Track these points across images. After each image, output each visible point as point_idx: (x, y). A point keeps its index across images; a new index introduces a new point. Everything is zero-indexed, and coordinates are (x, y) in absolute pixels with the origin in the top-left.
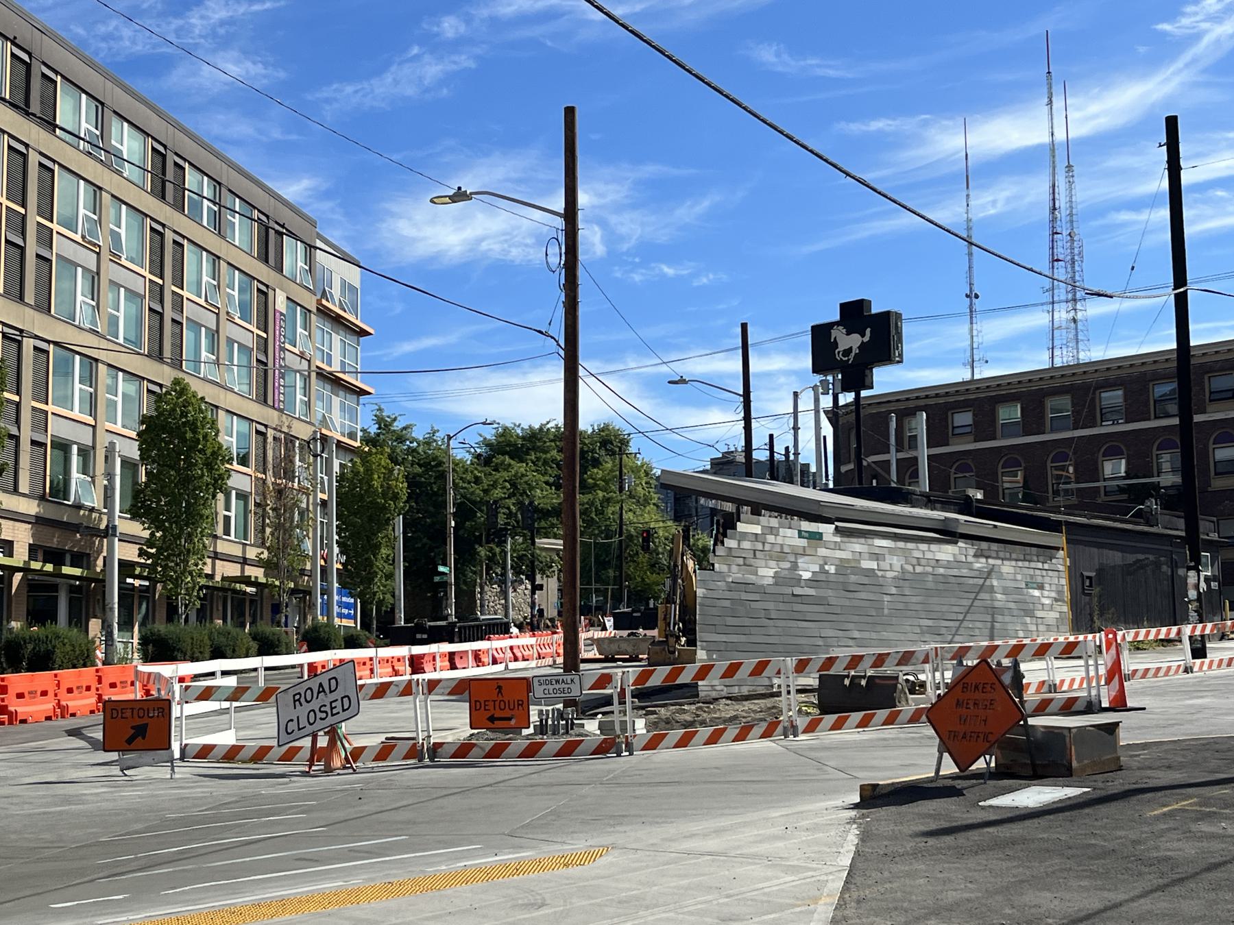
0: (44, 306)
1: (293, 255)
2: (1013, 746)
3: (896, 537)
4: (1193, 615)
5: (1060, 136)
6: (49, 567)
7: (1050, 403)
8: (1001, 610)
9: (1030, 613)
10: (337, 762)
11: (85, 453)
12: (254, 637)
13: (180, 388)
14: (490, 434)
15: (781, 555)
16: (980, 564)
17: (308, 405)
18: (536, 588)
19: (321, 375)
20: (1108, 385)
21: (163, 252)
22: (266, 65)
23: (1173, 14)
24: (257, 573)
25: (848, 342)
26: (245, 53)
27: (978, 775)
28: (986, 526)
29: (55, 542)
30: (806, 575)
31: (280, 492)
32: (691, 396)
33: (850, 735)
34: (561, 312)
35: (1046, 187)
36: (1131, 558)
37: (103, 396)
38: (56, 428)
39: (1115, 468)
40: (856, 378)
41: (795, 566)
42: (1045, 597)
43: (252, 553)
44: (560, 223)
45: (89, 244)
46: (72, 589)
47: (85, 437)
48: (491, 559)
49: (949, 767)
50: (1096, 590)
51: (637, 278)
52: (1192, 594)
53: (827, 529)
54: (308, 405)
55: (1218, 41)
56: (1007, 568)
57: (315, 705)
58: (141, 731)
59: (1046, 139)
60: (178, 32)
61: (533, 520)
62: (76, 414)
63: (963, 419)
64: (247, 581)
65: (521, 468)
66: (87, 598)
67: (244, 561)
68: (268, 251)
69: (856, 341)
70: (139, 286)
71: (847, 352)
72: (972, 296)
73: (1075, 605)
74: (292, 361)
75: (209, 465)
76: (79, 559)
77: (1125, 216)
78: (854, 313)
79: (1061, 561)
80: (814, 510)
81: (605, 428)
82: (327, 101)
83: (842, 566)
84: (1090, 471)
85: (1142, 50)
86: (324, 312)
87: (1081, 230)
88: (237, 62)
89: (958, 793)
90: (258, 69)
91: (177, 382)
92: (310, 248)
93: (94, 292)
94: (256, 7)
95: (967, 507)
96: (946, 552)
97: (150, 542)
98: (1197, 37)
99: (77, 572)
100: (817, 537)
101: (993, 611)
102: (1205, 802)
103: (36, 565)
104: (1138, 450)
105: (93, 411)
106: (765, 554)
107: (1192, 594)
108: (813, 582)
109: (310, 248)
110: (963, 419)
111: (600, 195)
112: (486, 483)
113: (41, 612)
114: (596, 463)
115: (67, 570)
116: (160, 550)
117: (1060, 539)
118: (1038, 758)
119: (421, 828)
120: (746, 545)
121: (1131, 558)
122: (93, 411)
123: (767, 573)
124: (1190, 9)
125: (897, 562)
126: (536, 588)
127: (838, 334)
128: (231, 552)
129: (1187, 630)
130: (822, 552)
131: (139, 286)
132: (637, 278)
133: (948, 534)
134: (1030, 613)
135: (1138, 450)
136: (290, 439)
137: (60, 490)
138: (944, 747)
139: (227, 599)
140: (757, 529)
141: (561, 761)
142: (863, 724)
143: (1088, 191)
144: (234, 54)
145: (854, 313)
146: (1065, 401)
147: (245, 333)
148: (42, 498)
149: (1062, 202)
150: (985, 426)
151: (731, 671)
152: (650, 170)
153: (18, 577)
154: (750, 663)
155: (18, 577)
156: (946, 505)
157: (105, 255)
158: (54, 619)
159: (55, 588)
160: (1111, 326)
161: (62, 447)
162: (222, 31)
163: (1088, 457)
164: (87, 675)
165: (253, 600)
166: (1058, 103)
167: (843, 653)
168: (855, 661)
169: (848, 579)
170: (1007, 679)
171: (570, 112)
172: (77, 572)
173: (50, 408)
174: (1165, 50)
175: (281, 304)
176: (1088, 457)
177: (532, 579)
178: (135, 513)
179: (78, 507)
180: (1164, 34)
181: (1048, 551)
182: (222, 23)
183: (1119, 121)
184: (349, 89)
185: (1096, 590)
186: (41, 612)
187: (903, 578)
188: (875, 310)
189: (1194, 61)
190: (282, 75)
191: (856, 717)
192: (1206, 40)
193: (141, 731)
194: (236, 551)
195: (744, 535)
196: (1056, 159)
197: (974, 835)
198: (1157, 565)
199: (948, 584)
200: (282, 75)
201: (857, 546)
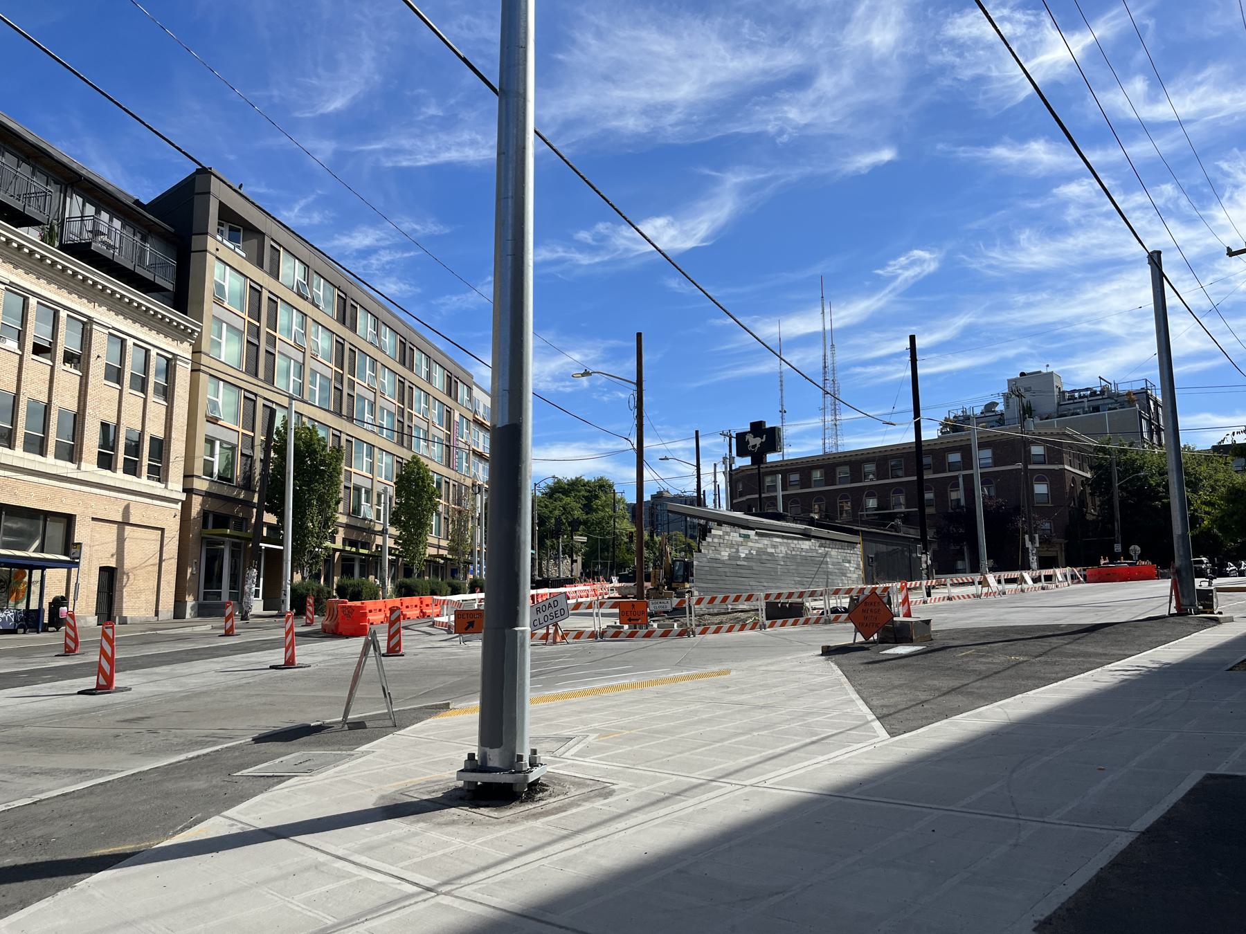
0: (350, 419)
1: (462, 391)
2: (886, 630)
3: (783, 537)
4: (924, 576)
5: (828, 327)
6: (354, 549)
7: (838, 470)
8: (831, 573)
9: (844, 574)
10: (558, 639)
11: (367, 492)
12: (450, 585)
13: (415, 461)
14: (550, 482)
15: (731, 546)
16: (821, 550)
17: (468, 467)
18: (573, 561)
19: (474, 451)
20: (868, 461)
21: (404, 391)
22: (411, 285)
23: (883, 265)
24: (444, 552)
25: (755, 441)
26: (400, 279)
27: (874, 642)
28: (824, 532)
29: (354, 537)
30: (743, 555)
31: (460, 512)
32: (690, 466)
33: (788, 629)
34: (635, 428)
35: (821, 353)
36: (891, 548)
37: (376, 463)
38: (356, 480)
39: (872, 503)
40: (758, 458)
41: (738, 551)
42: (851, 567)
43: (444, 543)
44: (635, 387)
45: (371, 389)
46: (362, 560)
47: (368, 484)
48: (553, 547)
49: (860, 638)
50: (875, 564)
51: (605, 399)
52: (924, 566)
53: (752, 533)
54: (468, 467)
55: (906, 280)
56: (834, 552)
57: (547, 613)
58: (471, 624)
59: (820, 329)
60: (365, 267)
61: (575, 525)
62: (364, 473)
63: (795, 477)
64: (441, 557)
65: (567, 500)
66: (372, 564)
67: (439, 547)
68: (451, 391)
69: (761, 438)
70: (393, 409)
71: (754, 446)
72: (783, 412)
73: (866, 571)
74: (461, 445)
75: (430, 499)
76: (366, 545)
77: (858, 370)
78: (757, 428)
79: (859, 549)
80: (744, 523)
81: (601, 479)
82: (444, 304)
83: (760, 551)
84: (858, 505)
85: (867, 283)
86: (476, 421)
87: (839, 375)
88: (395, 284)
89: (867, 649)
90: (405, 287)
91: (414, 457)
92: (470, 389)
93: (372, 412)
94: (406, 255)
95: (812, 522)
96: (806, 545)
97: (399, 537)
98: (895, 277)
99: (366, 552)
100: (747, 537)
101: (828, 573)
102: (979, 651)
103: (348, 548)
104: (882, 493)
105: (372, 471)
106: (726, 545)
107: (924, 566)
108: (746, 559)
109: (470, 389)
110: (795, 477)
111: (586, 355)
112: (551, 507)
113: (347, 570)
114: (597, 497)
115: (361, 551)
116: (405, 541)
117: (858, 539)
118: (901, 634)
119: (600, 667)
120: (716, 540)
121: (891, 548)
122: (372, 471)
123: (725, 554)
124: (892, 263)
125: (783, 549)
126: (573, 561)
127: (750, 438)
128: (435, 544)
129: (924, 583)
130: (750, 544)
131: (393, 409)
132: (605, 399)
133: (807, 536)
134: (844, 574)
135: (882, 493)
136: (460, 485)
137: (357, 511)
138: (857, 630)
139: (433, 565)
140: (720, 533)
141: (663, 639)
142: (794, 624)
143: (841, 356)
144: (394, 279)
145: (757, 428)
146: (847, 469)
147: (439, 432)
148: (349, 515)
149: (829, 362)
150: (806, 481)
151: (712, 600)
152: (613, 343)
153: (337, 554)
154: (720, 597)
155: (337, 554)
156: (802, 522)
157: (378, 394)
158: (353, 575)
159: (353, 560)
160: (854, 428)
161: (358, 489)
162: (387, 267)
163: (857, 497)
164: (379, 603)
165: (442, 566)
166: (827, 310)
167: (775, 592)
168: (779, 595)
169: (762, 557)
170: (885, 600)
171: (639, 335)
172: (366, 552)
173: (353, 470)
174: (879, 284)
175: (457, 417)
176: (857, 497)
177: (571, 556)
178: (395, 521)
179: (365, 519)
180: (879, 275)
181: (852, 544)
182: (388, 263)
183: (856, 320)
184: (454, 299)
185: (875, 564)
186: (347, 570)
187: (786, 557)
188: (767, 426)
189: (894, 290)
190: (419, 290)
191: (791, 620)
192: (900, 279)
193: (471, 624)
194: (435, 541)
195: (715, 536)
196: (826, 339)
197: (887, 663)
198: (903, 551)
199: (806, 560)
200: (419, 290)
201: (766, 541)
